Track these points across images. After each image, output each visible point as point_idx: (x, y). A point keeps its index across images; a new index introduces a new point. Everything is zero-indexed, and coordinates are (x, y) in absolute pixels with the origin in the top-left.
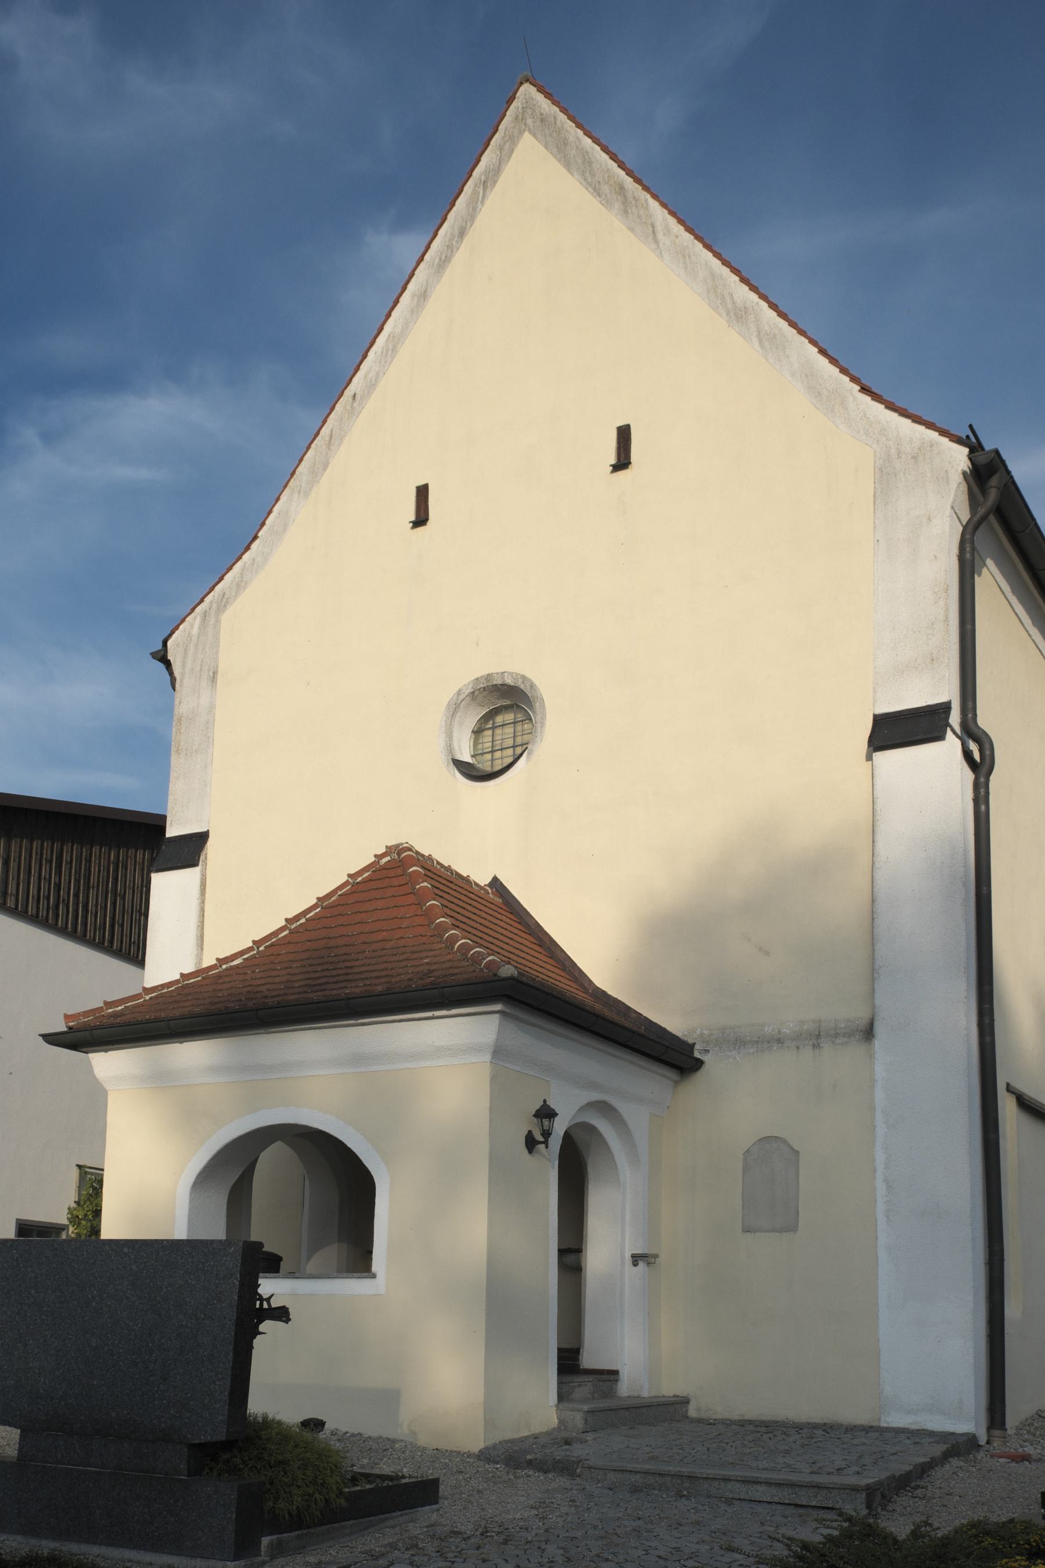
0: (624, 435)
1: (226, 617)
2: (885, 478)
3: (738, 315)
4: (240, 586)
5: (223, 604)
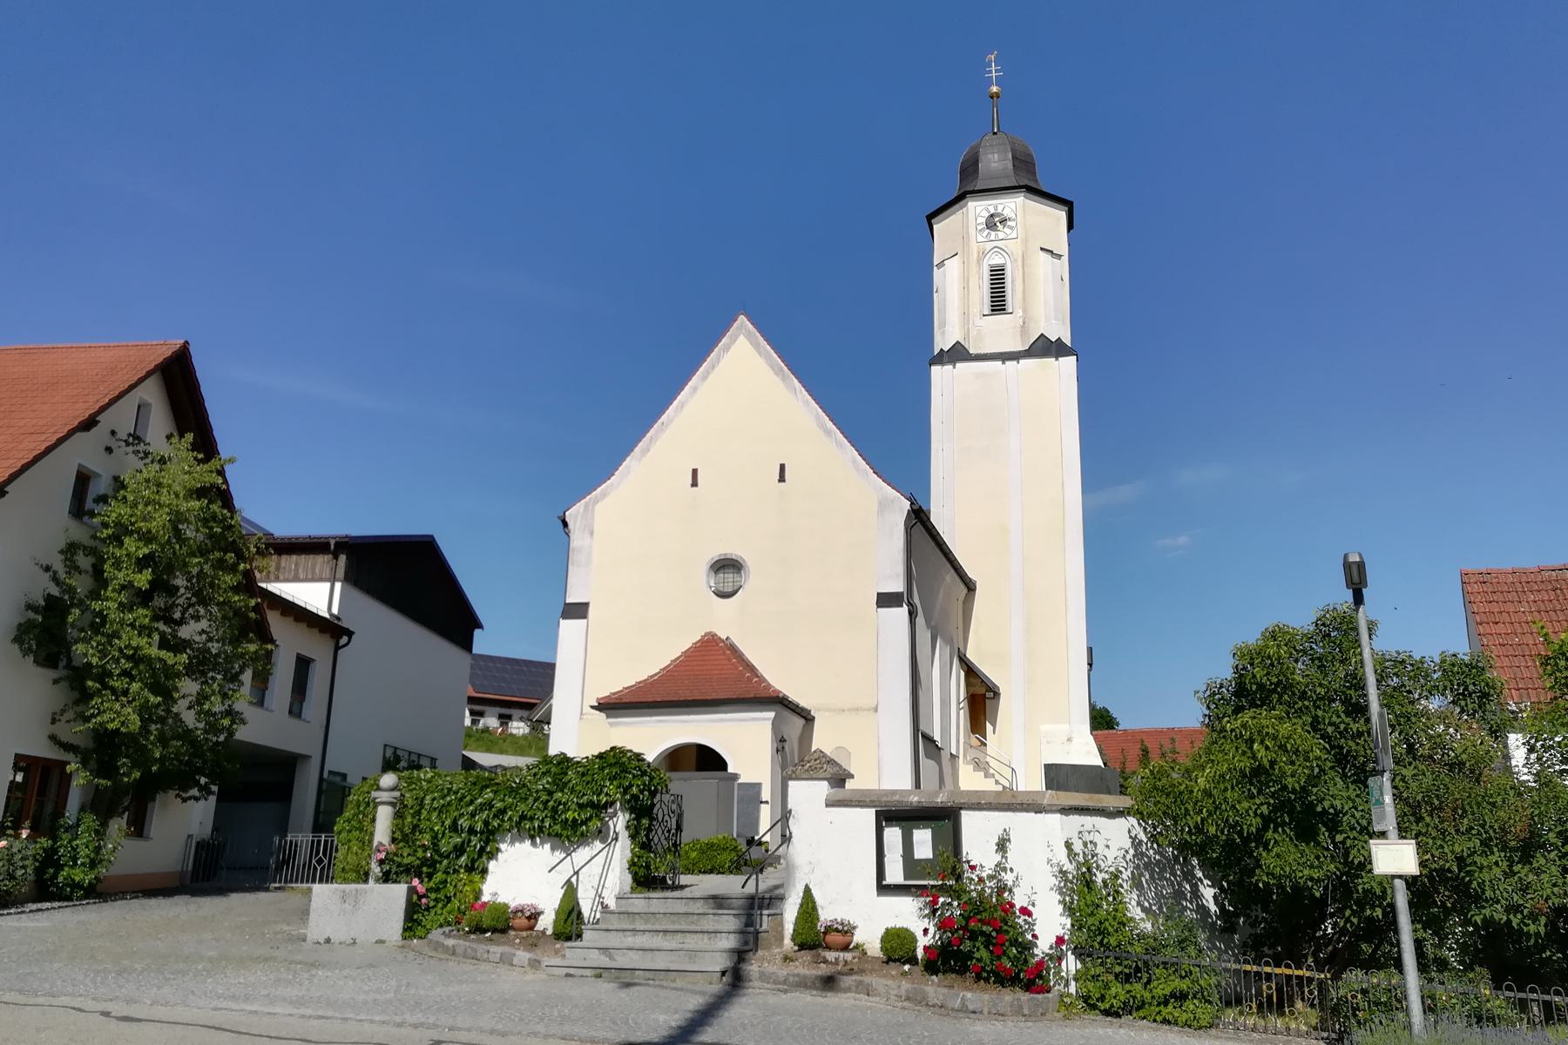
0: (782, 467)
1: (597, 507)
2: (883, 506)
3: (828, 432)
4: (604, 495)
5: (596, 501)
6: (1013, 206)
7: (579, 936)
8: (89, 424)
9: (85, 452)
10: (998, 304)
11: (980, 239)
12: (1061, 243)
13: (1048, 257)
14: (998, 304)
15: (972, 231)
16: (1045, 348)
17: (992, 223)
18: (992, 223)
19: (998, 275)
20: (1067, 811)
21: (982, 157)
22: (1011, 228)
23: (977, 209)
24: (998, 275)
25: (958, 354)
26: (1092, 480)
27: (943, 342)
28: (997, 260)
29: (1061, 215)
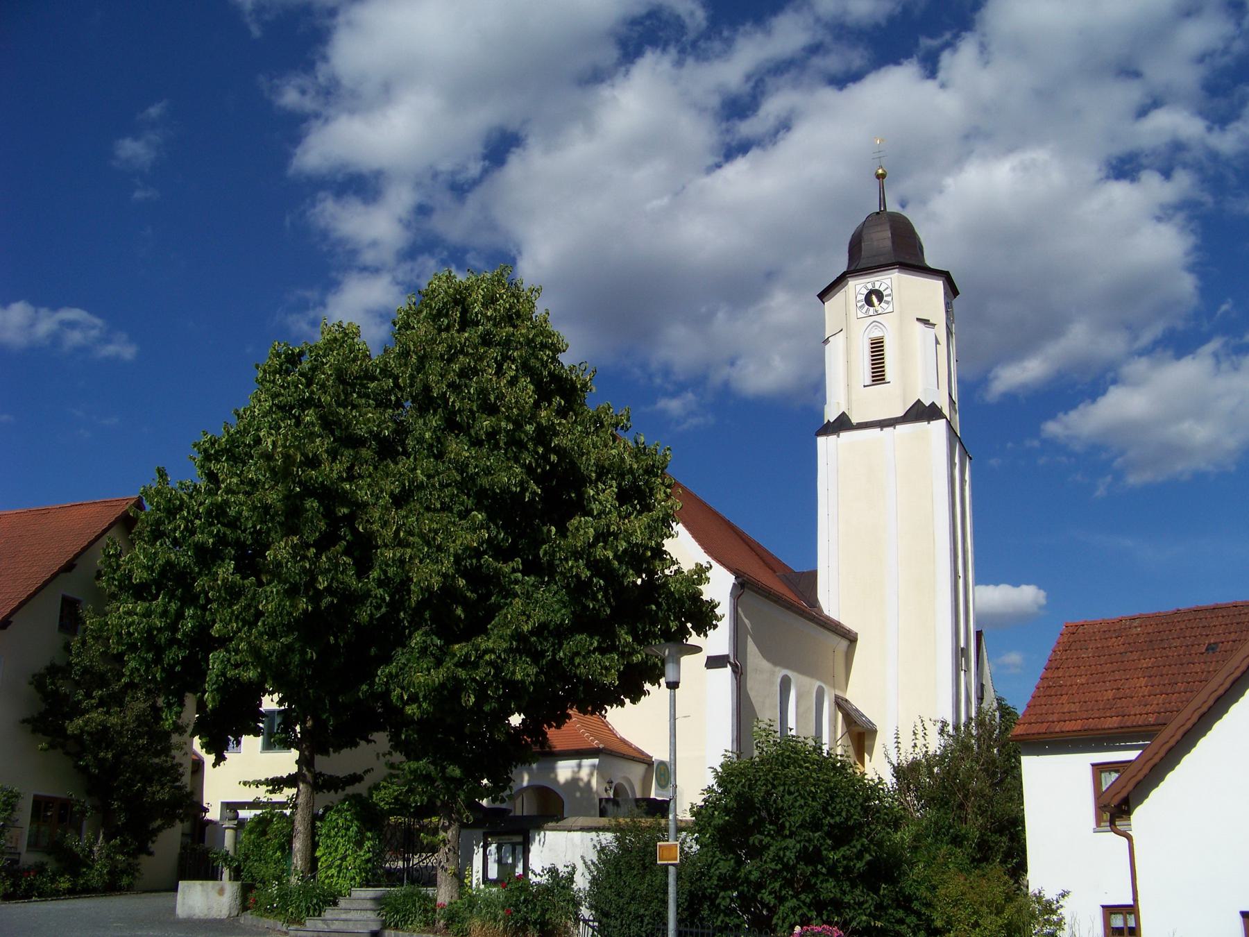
6: (888, 282)
7: (336, 904)
8: (69, 567)
9: (71, 587)
10: (878, 376)
11: (860, 315)
12: (938, 315)
13: (920, 326)
14: (878, 376)
15: (853, 308)
16: (921, 413)
17: (873, 296)
18: (873, 296)
19: (877, 347)
20: (582, 829)
21: (865, 237)
22: (887, 302)
23: (857, 287)
24: (877, 347)
25: (843, 424)
26: (824, 374)
27: (831, 415)
28: (876, 334)
29: (938, 285)
